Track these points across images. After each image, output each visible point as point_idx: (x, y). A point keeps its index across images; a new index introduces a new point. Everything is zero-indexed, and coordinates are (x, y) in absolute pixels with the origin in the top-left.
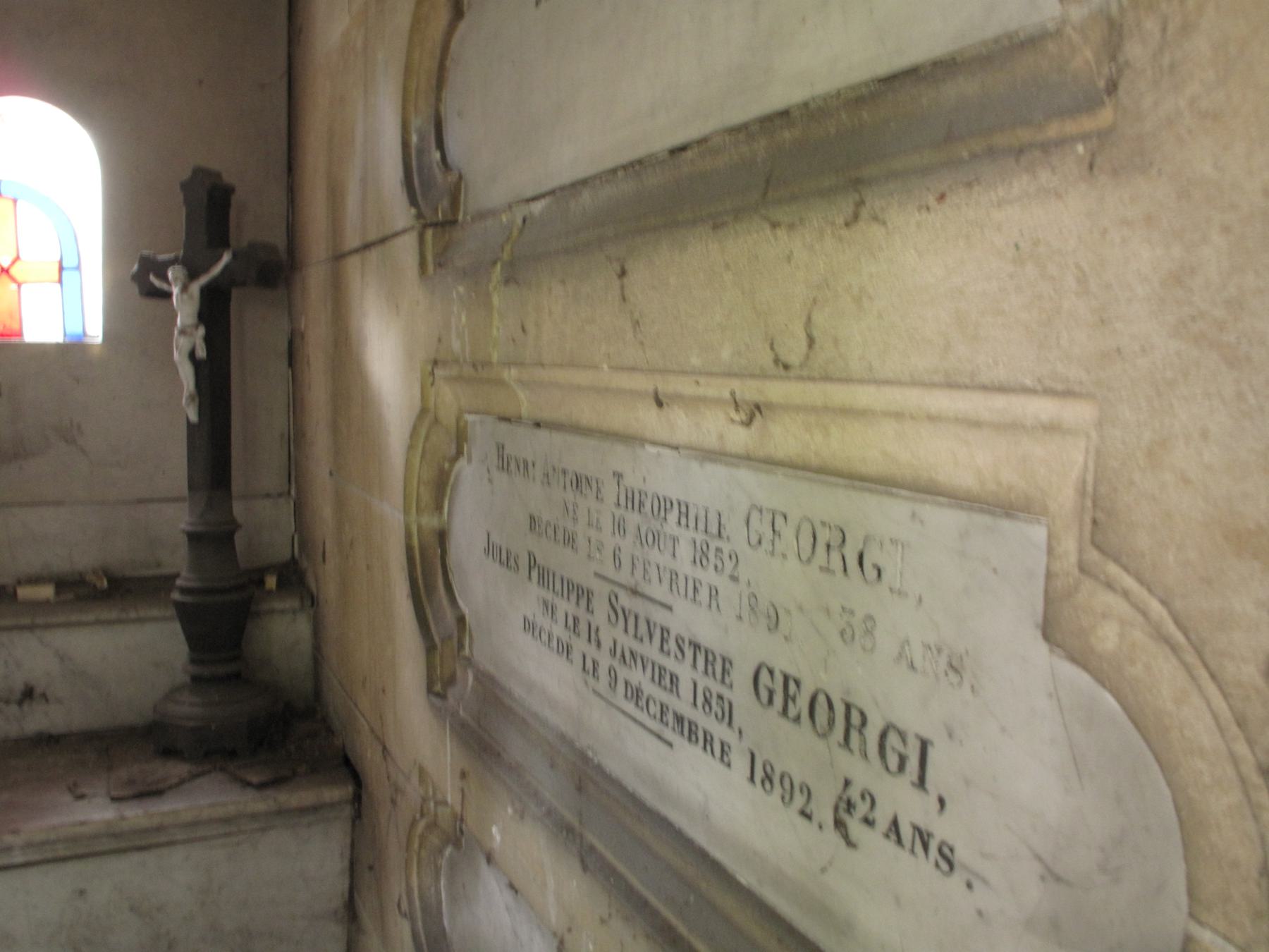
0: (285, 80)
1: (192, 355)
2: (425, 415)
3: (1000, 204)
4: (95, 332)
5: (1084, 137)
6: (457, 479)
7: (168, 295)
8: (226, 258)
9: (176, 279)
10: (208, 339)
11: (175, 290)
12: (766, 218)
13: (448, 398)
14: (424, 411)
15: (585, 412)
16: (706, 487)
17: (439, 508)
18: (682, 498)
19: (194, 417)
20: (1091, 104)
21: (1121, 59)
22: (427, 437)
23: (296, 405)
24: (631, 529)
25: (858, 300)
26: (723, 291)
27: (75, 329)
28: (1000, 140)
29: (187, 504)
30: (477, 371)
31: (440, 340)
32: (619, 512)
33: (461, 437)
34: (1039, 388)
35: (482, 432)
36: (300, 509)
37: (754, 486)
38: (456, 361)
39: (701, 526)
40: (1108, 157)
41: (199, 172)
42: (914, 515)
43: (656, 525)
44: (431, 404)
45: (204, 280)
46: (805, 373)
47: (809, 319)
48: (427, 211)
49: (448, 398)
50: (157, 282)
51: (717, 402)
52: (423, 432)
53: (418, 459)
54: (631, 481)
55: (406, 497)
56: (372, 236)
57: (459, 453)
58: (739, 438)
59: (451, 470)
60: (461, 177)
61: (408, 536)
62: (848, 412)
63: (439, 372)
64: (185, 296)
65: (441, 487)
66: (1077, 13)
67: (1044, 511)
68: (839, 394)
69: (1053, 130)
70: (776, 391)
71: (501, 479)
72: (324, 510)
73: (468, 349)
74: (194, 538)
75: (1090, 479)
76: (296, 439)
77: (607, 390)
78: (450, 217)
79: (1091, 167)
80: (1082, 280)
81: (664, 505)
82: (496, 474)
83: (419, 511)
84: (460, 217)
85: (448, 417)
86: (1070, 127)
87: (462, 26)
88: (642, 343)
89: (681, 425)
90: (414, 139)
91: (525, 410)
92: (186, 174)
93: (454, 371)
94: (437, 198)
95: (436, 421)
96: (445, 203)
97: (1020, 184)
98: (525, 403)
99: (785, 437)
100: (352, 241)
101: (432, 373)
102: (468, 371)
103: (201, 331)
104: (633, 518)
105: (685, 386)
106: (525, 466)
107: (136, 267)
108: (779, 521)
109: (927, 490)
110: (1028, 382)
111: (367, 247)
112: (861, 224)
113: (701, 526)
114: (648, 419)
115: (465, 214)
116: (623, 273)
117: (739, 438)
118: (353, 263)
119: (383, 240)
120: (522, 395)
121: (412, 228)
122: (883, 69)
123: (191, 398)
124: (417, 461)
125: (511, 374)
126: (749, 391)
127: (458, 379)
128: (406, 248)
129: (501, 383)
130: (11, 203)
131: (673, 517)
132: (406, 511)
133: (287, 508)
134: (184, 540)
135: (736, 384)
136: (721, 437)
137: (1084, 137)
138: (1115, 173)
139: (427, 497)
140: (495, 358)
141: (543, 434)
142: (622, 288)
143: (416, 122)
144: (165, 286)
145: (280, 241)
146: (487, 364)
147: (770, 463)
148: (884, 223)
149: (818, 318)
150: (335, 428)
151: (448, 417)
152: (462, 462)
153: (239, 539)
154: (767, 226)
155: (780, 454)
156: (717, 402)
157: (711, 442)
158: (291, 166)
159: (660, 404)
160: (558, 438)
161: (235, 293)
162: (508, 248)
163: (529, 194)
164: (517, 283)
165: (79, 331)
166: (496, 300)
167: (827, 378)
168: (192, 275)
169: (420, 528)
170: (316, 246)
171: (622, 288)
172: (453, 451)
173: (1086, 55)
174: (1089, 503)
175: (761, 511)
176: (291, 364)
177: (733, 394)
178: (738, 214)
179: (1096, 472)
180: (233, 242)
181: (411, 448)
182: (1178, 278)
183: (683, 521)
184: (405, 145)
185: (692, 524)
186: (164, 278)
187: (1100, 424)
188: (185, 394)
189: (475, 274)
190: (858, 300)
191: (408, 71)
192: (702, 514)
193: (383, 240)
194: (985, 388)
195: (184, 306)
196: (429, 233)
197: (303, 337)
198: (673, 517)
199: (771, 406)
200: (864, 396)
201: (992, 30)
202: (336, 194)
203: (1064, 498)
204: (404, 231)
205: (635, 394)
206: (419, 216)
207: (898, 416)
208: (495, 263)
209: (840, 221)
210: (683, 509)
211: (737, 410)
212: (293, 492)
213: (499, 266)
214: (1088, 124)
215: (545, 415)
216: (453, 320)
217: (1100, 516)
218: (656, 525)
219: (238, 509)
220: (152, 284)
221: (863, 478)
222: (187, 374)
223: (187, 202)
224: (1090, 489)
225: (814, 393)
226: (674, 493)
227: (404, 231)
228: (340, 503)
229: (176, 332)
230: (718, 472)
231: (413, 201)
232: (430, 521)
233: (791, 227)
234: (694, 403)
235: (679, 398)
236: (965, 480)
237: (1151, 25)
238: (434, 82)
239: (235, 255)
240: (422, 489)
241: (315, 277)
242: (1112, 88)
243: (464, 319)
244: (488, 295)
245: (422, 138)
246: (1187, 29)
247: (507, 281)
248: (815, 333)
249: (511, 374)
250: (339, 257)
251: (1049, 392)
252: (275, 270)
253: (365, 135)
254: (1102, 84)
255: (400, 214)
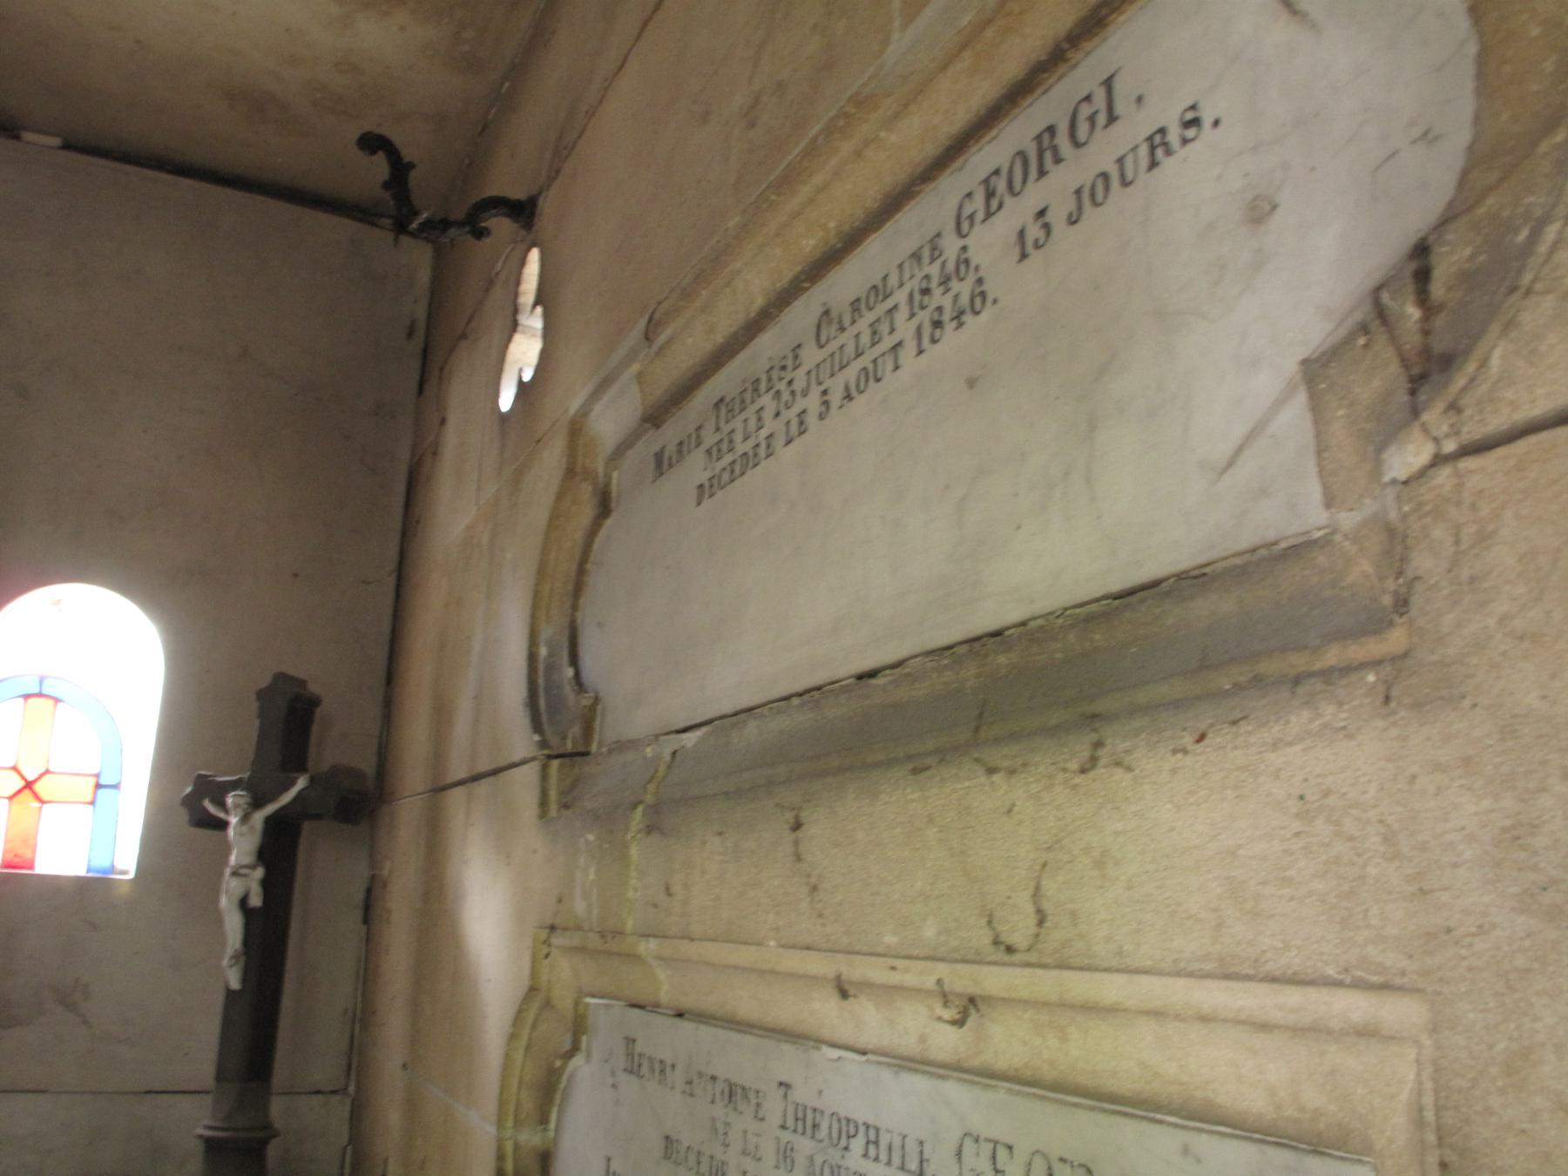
0: (394, 575)
1: (243, 903)
2: (534, 994)
3: (1276, 745)
4: (125, 859)
5: (1375, 664)
6: (570, 1080)
7: (222, 825)
8: (301, 783)
9: (236, 806)
10: (265, 883)
11: (234, 820)
12: (977, 760)
13: (565, 974)
14: (533, 989)
15: (745, 1000)
16: (899, 1104)
17: (544, 1120)
18: (871, 1121)
19: (235, 984)
20: (1376, 624)
21: (1410, 574)
22: (534, 1027)
23: (368, 974)
24: (801, 1161)
25: (1099, 864)
26: (924, 852)
27: (102, 862)
28: (1268, 667)
29: (208, 1100)
30: (606, 943)
31: (560, 901)
32: (786, 1136)
33: (579, 1026)
34: (1348, 980)
35: (607, 1019)
36: (359, 1112)
37: (964, 1105)
38: (579, 928)
39: (896, 1160)
40: (1409, 688)
41: (281, 678)
42: (1186, 1151)
43: (834, 1155)
44: (544, 978)
45: (270, 809)
46: (1033, 957)
47: (1037, 888)
48: (554, 741)
49: (565, 974)
50: (212, 809)
51: (918, 992)
52: (530, 1016)
53: (521, 1051)
54: (801, 1094)
55: (502, 1104)
56: (484, 765)
57: (575, 1048)
58: (946, 1041)
59: (563, 1068)
60: (597, 699)
61: (500, 1157)
62: (1090, 1009)
63: (557, 940)
64: (245, 829)
65: (548, 1090)
66: (1348, 520)
67: (1368, 1149)
68: (1079, 986)
69: (1332, 656)
70: (994, 980)
71: (628, 1083)
72: (390, 1115)
73: (595, 912)
74: (213, 1147)
75: (1428, 1100)
76: (363, 1018)
77: (772, 972)
78: (582, 749)
79: (1387, 699)
80: (1389, 838)
81: (847, 1128)
82: (623, 1077)
83: (518, 1123)
84: (594, 748)
85: (564, 1000)
86: (1357, 651)
87: (609, 522)
88: (820, 916)
89: (869, 1022)
90: (543, 651)
91: (665, 995)
92: (265, 681)
93: (575, 940)
94: (566, 723)
95: (548, 1004)
96: (576, 730)
97: (1299, 719)
98: (667, 986)
99: (1008, 1041)
100: (458, 771)
101: (546, 942)
102: (594, 941)
103: (259, 873)
104: (804, 1145)
105: (875, 971)
106: (662, 1069)
107: (189, 789)
108: (1002, 1154)
109: (1201, 1115)
110: (1331, 972)
111: (476, 778)
112: (1099, 771)
113: (896, 1160)
114: (826, 1012)
115: (600, 745)
116: (797, 826)
117: (946, 1041)
118: (457, 796)
119: (496, 772)
120: (661, 974)
121: (534, 759)
122: (1116, 586)
123: (235, 957)
124: (519, 1056)
125: (648, 947)
126: (962, 979)
127: (581, 949)
128: (524, 782)
129: (633, 957)
130: (101, 791)
131: (858, 1144)
132: (500, 1123)
133: (340, 1110)
134: (199, 1147)
135: (942, 970)
136: (923, 1039)
137: (1375, 664)
138: (1417, 706)
139: (528, 1105)
140: (630, 925)
141: (686, 1026)
142: (796, 842)
143: (546, 633)
144: (222, 815)
145: (367, 764)
146: (619, 933)
147: (989, 1076)
148: (1129, 769)
149: (1050, 886)
150: (415, 1008)
151: (564, 1000)
152: (578, 1061)
153: (273, 1151)
154: (981, 771)
155: (1001, 1064)
156: (918, 992)
157: (908, 1043)
158: (391, 677)
159: (844, 994)
160: (705, 1032)
161: (307, 827)
162: (651, 788)
163: (682, 725)
164: (663, 834)
165: (106, 864)
166: (634, 851)
167: (1063, 966)
168: (257, 804)
169: (517, 1147)
170: (412, 775)
171: (796, 842)
172: (567, 1046)
173: (1363, 568)
174: (1431, 1138)
175: (977, 1140)
176: (366, 920)
177: (939, 982)
178: (945, 755)
179: (1436, 1091)
180: (310, 764)
181: (513, 1037)
182: (1515, 835)
183: (872, 1151)
184: (532, 658)
185: (883, 1157)
186: (222, 805)
187: (1434, 1029)
188: (229, 951)
189: (609, 819)
190: (1099, 864)
191: (541, 573)
192: (897, 1142)
193: (496, 772)
194: (1274, 980)
195: (242, 838)
196: (555, 763)
197: (385, 885)
198: (858, 1144)
199: (989, 999)
200: (1112, 988)
201: (1246, 540)
202: (442, 712)
203: (1393, 1129)
204: (524, 762)
205: (813, 980)
206: (543, 744)
207: (1158, 1014)
208: (635, 806)
209: (1074, 765)
210: (872, 1136)
211: (946, 1004)
212: (352, 1089)
213: (640, 809)
214: (1374, 648)
215: (687, 1002)
216: (579, 874)
217: (1451, 1157)
218: (834, 1155)
219: (277, 1108)
220: (205, 811)
221: (1113, 1098)
222: (234, 925)
223: (262, 714)
224: (1429, 1115)
225: (1046, 984)
226: (861, 1116)
227: (524, 762)
228: (413, 1106)
229: (228, 872)
230: (919, 1083)
231: (537, 726)
232: (530, 1138)
233: (1012, 772)
234: (889, 993)
235: (867, 986)
236: (1253, 1102)
237: (1439, 533)
238: (570, 587)
239: (312, 780)
240: (524, 1095)
241: (407, 813)
242: (1402, 604)
243: (592, 876)
244: (625, 846)
245: (552, 646)
246: (1484, 538)
247: (649, 829)
248: (1047, 906)
249: (648, 947)
250: (440, 789)
251: (1359, 985)
252: (358, 802)
253: (484, 643)
254: (1387, 600)
255: (520, 741)
